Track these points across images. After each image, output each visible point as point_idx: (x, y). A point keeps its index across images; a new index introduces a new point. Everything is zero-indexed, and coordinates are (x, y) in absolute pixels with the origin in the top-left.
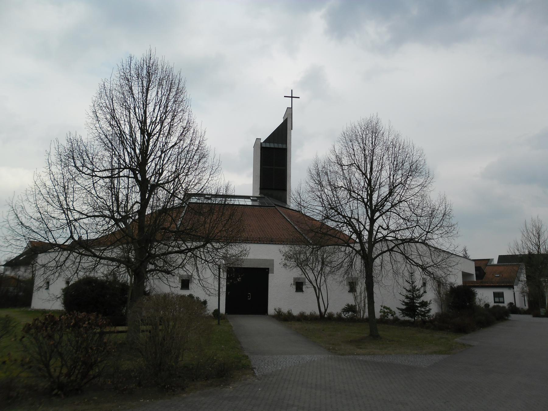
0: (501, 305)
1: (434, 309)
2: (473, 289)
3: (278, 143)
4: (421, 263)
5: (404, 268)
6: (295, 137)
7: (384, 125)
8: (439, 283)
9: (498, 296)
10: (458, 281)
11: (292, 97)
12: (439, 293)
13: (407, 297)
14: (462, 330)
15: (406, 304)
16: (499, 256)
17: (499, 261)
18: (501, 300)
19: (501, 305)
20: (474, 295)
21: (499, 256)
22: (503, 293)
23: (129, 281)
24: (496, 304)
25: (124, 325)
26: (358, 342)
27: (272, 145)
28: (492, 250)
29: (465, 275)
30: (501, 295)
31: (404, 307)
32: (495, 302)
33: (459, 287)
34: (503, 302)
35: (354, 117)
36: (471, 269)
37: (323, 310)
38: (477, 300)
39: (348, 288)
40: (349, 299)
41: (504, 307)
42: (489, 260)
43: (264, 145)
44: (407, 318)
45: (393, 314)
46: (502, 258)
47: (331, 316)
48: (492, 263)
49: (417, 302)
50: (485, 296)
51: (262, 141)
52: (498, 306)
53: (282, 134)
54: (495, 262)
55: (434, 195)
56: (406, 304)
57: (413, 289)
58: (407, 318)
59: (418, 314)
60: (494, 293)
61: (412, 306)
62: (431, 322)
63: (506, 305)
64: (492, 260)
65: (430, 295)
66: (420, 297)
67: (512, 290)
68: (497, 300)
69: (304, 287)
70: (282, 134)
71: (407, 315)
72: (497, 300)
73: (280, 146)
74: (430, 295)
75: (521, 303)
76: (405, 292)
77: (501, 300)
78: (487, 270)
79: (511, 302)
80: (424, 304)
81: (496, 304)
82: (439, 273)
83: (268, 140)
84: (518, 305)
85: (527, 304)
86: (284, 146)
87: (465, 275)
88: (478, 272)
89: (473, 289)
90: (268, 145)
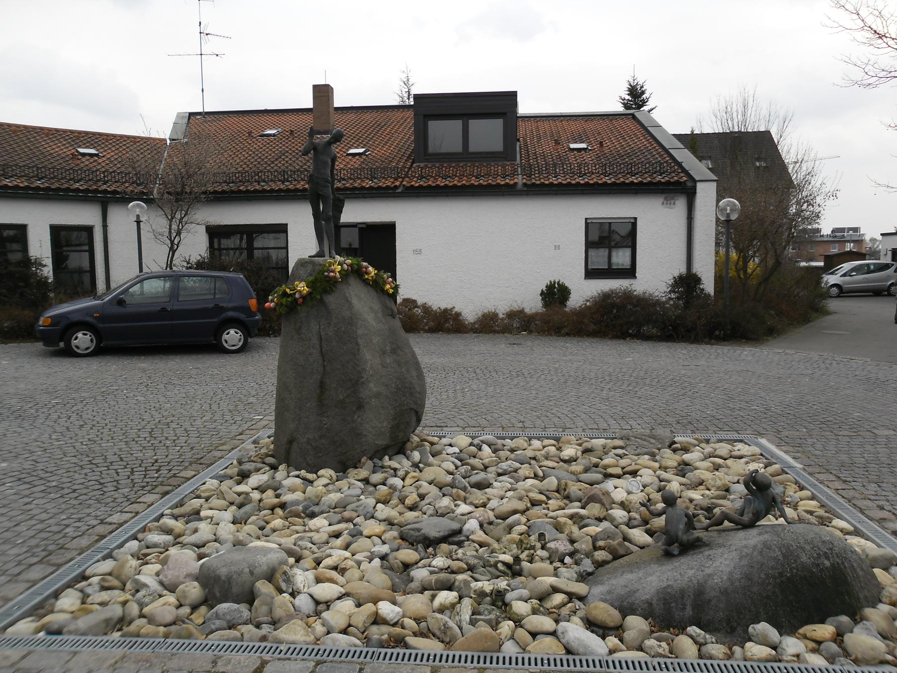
16: (315, 87)
18: (621, 258)
21: (315, 87)
30: (624, 236)
32: (591, 274)
34: (630, 272)
68: (599, 258)
72: (599, 258)
77: (621, 258)
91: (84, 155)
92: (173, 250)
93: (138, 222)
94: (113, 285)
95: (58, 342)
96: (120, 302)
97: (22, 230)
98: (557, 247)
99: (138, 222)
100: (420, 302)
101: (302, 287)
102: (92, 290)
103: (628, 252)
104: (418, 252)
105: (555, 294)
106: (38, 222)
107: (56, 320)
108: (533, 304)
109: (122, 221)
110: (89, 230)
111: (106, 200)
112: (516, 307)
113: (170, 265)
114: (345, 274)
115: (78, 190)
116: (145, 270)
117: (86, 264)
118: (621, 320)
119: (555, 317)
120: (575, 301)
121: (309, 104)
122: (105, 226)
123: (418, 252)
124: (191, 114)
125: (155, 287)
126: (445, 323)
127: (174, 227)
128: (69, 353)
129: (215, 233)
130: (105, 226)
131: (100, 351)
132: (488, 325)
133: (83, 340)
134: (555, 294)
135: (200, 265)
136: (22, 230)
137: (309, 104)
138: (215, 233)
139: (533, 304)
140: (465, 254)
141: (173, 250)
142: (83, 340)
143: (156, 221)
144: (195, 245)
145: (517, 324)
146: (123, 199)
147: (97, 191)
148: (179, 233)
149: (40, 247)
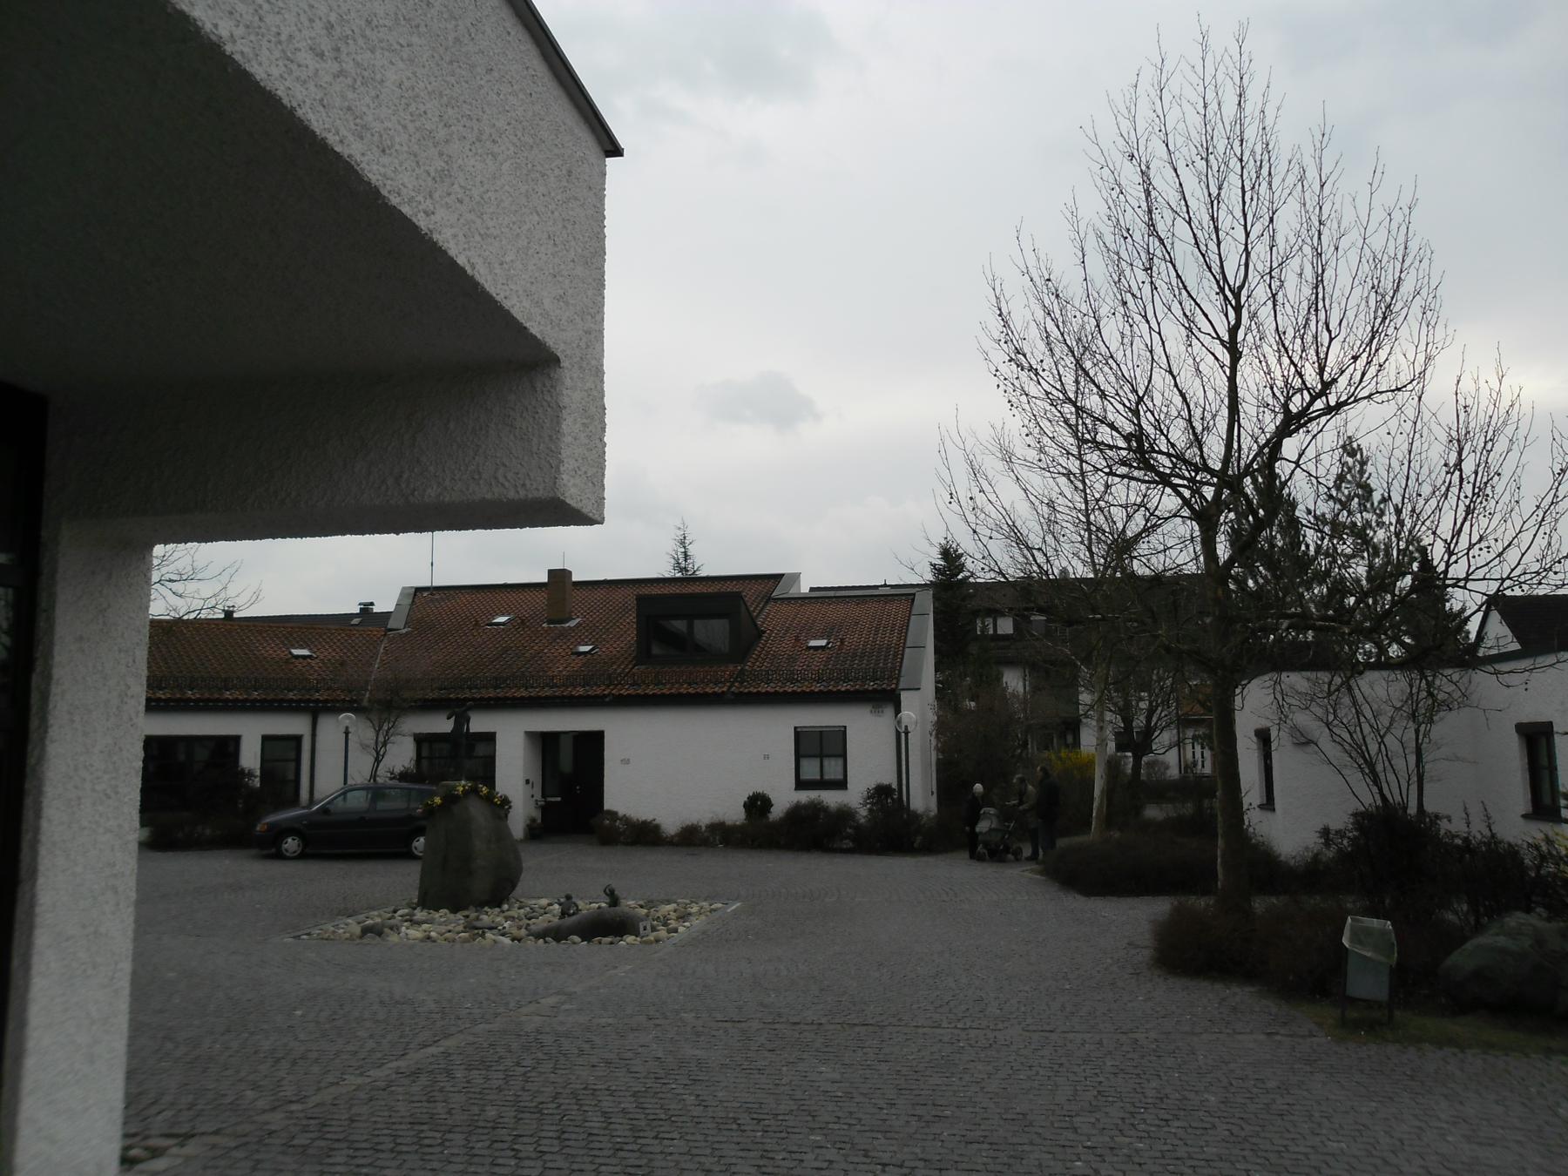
0: (831, 798)
9: (820, 748)
18: (832, 769)
19: (831, 798)
22: (842, 733)
23: (1021, 690)
24: (805, 796)
25: (1205, 892)
32: (801, 784)
34: (841, 784)
35: (559, 349)
41: (845, 814)
42: (778, 578)
48: (793, 592)
52: (816, 808)
60: (799, 734)
63: (853, 797)
67: (889, 711)
68: (811, 770)
77: (832, 769)
79: (886, 782)
81: (805, 796)
88: (202, 754)
89: (1516, 646)
91: (297, 657)
92: (378, 761)
93: (347, 733)
94: (317, 795)
95: (269, 847)
96: (325, 810)
97: (237, 740)
98: (766, 757)
99: (347, 733)
100: (621, 813)
101: (438, 800)
102: (294, 801)
103: (840, 762)
104: (626, 762)
105: (758, 805)
106: (251, 733)
107: (272, 826)
108: (734, 813)
109: (331, 729)
110: (298, 739)
111: (316, 710)
112: (716, 820)
113: (374, 776)
114: (466, 793)
115: (291, 700)
116: (350, 782)
117: (291, 776)
118: (810, 832)
119: (759, 830)
120: (778, 811)
121: (544, 579)
122: (314, 735)
123: (626, 762)
124: (418, 590)
125: (358, 801)
126: (644, 835)
127: (381, 739)
128: (279, 856)
129: (420, 740)
130: (314, 735)
131: (302, 856)
132: (691, 838)
133: (291, 844)
134: (758, 805)
135: (404, 776)
136: (237, 740)
137: (544, 579)
138: (420, 740)
139: (734, 813)
140: (680, 763)
141: (378, 761)
142: (291, 844)
143: (363, 731)
144: (402, 755)
145: (719, 837)
146: (333, 707)
147: (309, 701)
148: (385, 744)
149: (250, 758)
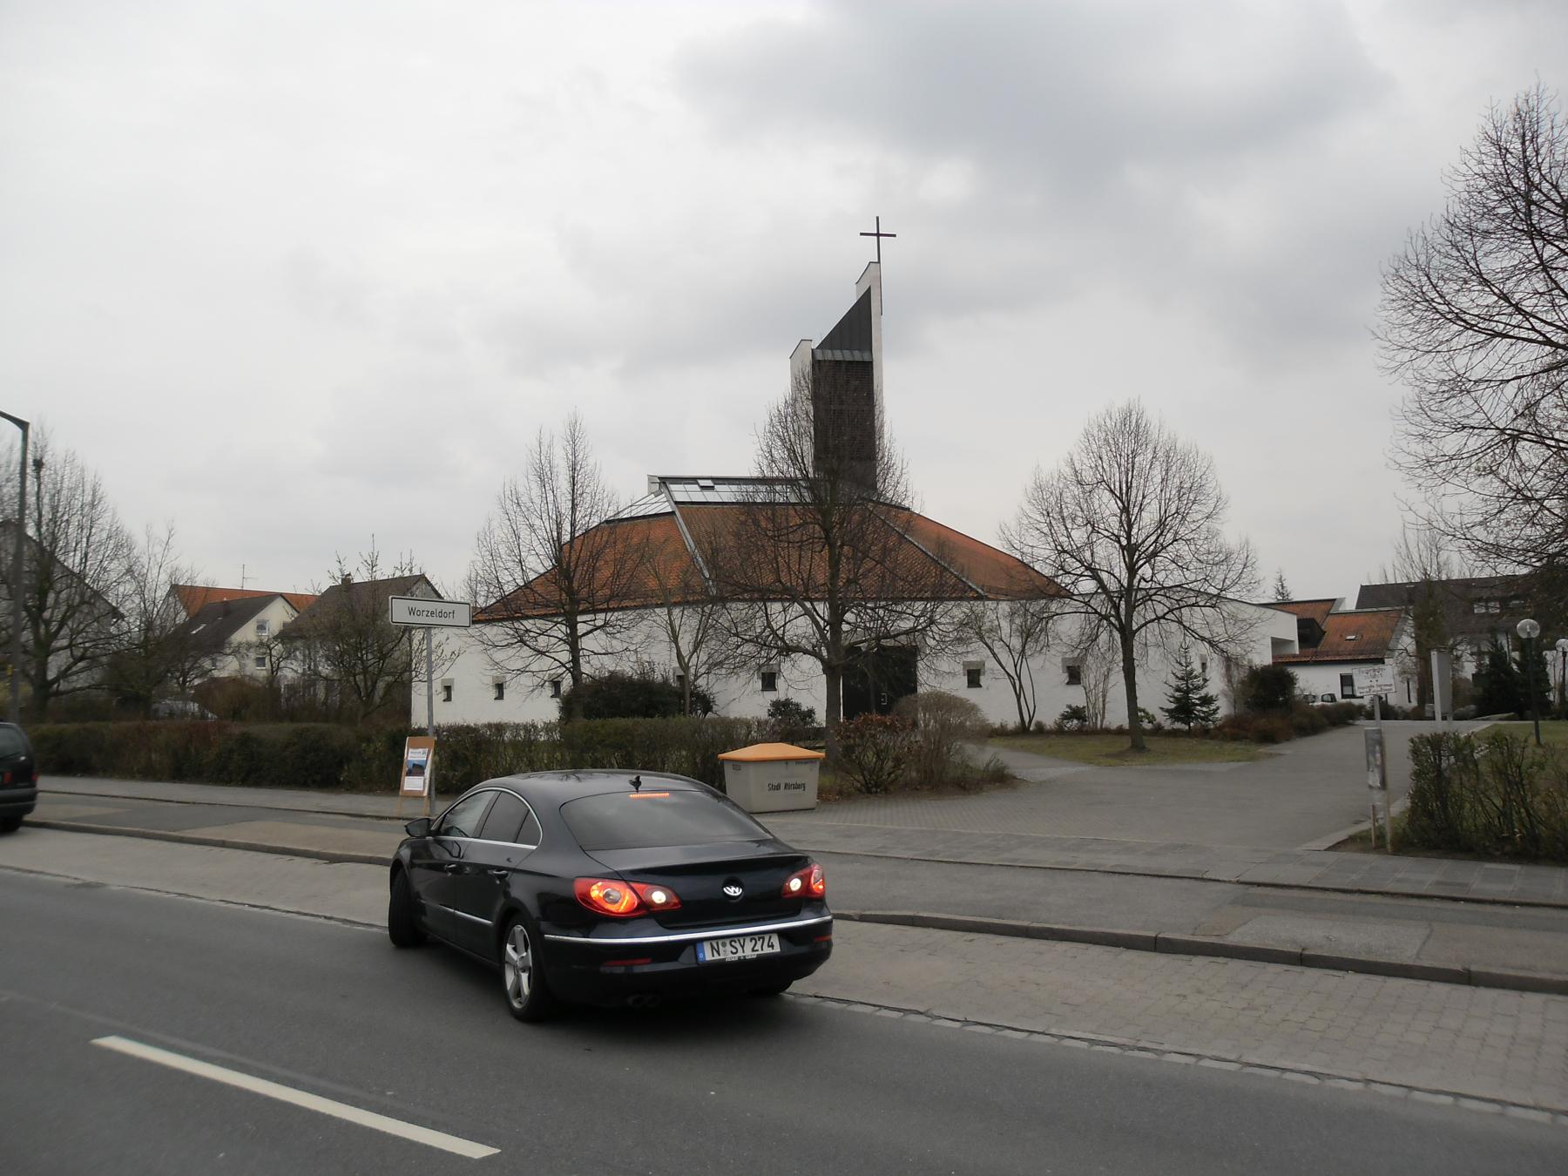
1: (1223, 709)
2: (1291, 670)
3: (851, 349)
4: (1207, 635)
5: (1177, 637)
6: (885, 330)
7: (1152, 417)
8: (1229, 662)
10: (1262, 657)
11: (878, 235)
12: (1230, 681)
13: (1178, 689)
14: (1268, 738)
15: (1177, 700)
17: (1361, 602)
20: (1291, 681)
26: (1120, 755)
27: (838, 355)
28: (1338, 580)
29: (1277, 643)
31: (1173, 706)
32: (1344, 696)
33: (1265, 669)
36: (1288, 628)
37: (1027, 719)
38: (1297, 692)
39: (1065, 677)
40: (1076, 696)
43: (819, 357)
44: (1178, 725)
45: (1151, 719)
46: (1370, 595)
47: (1041, 730)
48: (1341, 609)
49: (1194, 697)
50: (1317, 683)
51: (815, 345)
52: (1350, 704)
53: (857, 327)
54: (1350, 604)
55: (1230, 532)
56: (1177, 700)
57: (1188, 676)
58: (1178, 725)
59: (1197, 717)
60: (1342, 677)
61: (1183, 708)
62: (1219, 728)
64: (1342, 600)
65: (1216, 685)
66: (1198, 688)
69: (982, 678)
70: (857, 327)
71: (1178, 719)
73: (857, 356)
74: (1216, 685)
75: (1398, 697)
76: (1174, 682)
78: (1328, 625)
80: (1207, 700)
82: (1233, 649)
83: (828, 343)
84: (1393, 700)
85: (1414, 695)
86: (866, 359)
87: (1277, 643)
89: (1291, 670)
90: (829, 355)
